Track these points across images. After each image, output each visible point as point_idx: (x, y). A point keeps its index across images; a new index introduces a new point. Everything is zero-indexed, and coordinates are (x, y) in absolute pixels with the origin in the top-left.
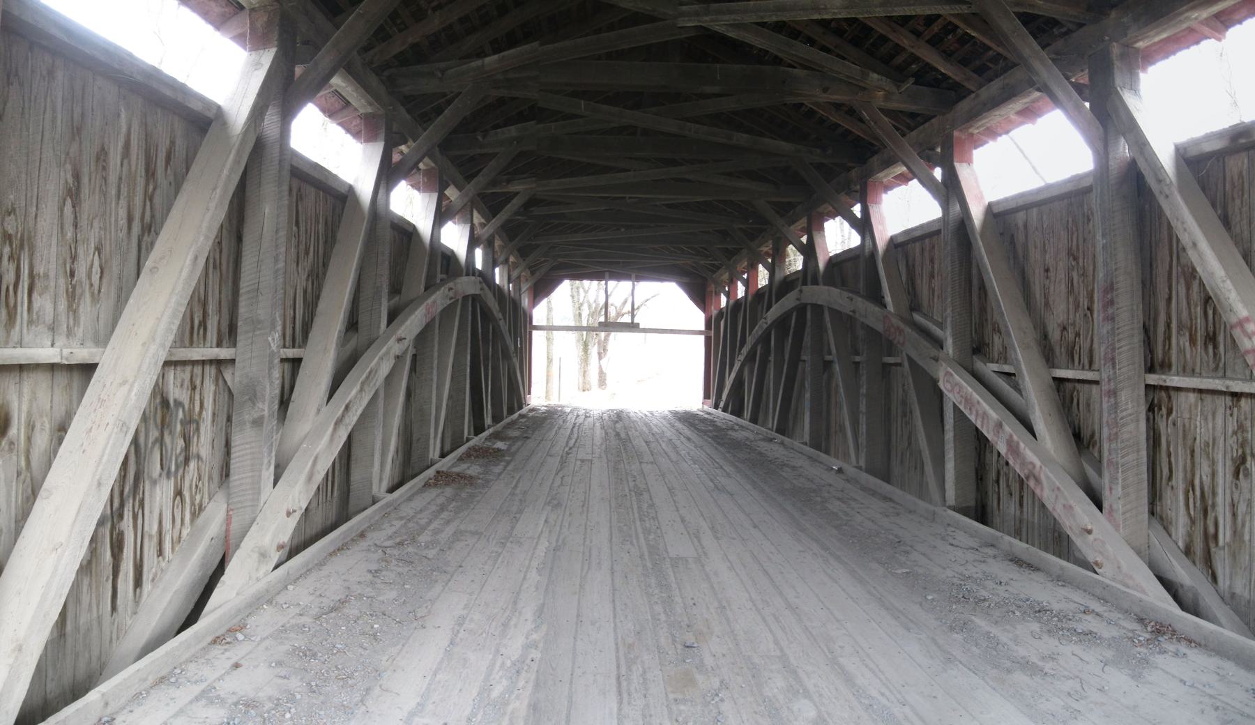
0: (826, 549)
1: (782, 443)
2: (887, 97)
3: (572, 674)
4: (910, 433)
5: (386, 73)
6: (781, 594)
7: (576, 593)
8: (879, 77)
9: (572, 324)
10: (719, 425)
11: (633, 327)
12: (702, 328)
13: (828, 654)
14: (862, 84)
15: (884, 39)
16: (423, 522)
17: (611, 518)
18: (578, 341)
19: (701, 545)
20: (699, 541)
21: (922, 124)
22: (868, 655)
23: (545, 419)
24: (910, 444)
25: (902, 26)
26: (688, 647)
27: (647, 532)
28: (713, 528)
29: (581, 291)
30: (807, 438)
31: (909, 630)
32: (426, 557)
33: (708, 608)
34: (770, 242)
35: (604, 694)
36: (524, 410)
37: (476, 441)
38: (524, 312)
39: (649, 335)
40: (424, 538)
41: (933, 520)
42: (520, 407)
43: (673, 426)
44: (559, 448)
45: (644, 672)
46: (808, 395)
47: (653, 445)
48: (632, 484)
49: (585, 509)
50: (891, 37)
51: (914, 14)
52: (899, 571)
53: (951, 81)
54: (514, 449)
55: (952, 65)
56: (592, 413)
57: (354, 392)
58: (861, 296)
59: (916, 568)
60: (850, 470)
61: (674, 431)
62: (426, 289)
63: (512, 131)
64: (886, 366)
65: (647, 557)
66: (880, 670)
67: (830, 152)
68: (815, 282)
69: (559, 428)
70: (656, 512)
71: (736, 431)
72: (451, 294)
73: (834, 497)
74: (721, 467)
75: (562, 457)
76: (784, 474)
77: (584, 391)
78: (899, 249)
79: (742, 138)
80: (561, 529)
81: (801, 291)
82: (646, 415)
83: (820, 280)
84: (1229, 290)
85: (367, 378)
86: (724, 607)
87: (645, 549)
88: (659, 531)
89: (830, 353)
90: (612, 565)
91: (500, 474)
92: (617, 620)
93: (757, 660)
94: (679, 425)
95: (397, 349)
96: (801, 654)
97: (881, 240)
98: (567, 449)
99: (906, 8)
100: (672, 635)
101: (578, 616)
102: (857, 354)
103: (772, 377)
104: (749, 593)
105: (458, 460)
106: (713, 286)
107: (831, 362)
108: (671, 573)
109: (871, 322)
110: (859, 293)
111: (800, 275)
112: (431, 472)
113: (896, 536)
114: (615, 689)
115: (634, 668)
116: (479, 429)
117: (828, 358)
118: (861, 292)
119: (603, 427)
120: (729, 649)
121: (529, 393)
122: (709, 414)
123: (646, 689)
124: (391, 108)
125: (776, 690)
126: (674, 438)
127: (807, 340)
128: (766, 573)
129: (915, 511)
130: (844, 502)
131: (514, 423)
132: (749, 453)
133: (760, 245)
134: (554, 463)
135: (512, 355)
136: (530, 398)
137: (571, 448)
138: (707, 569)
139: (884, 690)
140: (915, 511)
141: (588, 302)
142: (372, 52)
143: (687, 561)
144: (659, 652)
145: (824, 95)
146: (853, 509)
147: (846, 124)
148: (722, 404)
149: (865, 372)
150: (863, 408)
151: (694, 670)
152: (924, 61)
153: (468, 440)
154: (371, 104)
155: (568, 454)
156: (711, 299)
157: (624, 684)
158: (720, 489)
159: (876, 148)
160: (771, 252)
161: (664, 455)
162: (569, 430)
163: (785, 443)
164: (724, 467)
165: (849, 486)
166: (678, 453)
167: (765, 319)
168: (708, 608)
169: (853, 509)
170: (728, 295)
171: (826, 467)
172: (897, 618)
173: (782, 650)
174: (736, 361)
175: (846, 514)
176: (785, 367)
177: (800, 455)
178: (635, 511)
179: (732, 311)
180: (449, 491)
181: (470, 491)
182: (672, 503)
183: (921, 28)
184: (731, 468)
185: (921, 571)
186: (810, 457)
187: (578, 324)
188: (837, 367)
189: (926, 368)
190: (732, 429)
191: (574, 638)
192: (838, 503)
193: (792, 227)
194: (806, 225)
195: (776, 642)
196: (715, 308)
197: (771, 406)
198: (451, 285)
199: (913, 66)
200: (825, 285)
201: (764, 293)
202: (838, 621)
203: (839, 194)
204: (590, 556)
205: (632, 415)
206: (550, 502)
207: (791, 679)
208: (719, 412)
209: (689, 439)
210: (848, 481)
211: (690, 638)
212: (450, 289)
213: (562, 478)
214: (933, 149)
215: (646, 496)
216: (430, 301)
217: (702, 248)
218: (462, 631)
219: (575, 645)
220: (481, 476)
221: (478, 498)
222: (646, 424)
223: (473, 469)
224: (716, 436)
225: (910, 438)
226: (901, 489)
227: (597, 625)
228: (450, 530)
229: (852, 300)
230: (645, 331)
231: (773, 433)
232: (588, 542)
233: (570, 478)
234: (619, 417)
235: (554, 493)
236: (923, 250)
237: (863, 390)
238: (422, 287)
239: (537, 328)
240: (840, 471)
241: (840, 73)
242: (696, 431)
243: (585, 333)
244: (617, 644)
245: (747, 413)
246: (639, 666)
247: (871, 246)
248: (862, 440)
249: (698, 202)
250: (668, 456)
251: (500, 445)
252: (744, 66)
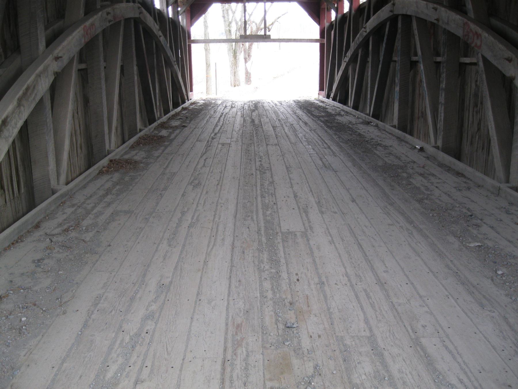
0: (411, 222)
1: (377, 126)
3: (183, 359)
4: (480, 120)
6: (372, 268)
7: (199, 270)
9: (225, 38)
10: (330, 111)
11: (266, 38)
12: (318, 37)
13: (411, 334)
16: (89, 207)
17: (238, 196)
18: (229, 50)
19: (308, 219)
20: (307, 216)
22: (447, 336)
23: (201, 110)
24: (479, 129)
26: (288, 327)
27: (265, 207)
28: (319, 203)
29: (230, 12)
30: (396, 122)
31: (482, 306)
32: (83, 240)
33: (309, 285)
35: (209, 381)
36: (187, 104)
37: (146, 131)
38: (183, 28)
39: (283, 44)
40: (85, 223)
41: (498, 195)
42: (184, 102)
43: (295, 113)
44: (206, 136)
45: (247, 356)
46: (397, 89)
47: (278, 130)
48: (258, 164)
49: (219, 187)
52: (472, 245)
54: (173, 136)
56: (236, 104)
57: (10, 108)
59: (486, 241)
60: (430, 149)
61: (295, 117)
62: (86, 14)
64: (463, 66)
65: (262, 232)
66: (458, 353)
69: (210, 117)
70: (275, 189)
71: (342, 116)
72: (110, 17)
73: (417, 173)
74: (329, 148)
75: (208, 142)
76: (377, 152)
77: (235, 86)
80: (197, 206)
82: (276, 105)
84: (160, 36)
85: (25, 94)
86: (323, 283)
87: (262, 224)
88: (275, 207)
89: (416, 55)
90: (234, 241)
91: (158, 157)
92: (231, 298)
93: (348, 342)
94: (300, 112)
95: (55, 67)
96: (388, 334)
98: (213, 135)
100: (276, 314)
101: (198, 294)
102: (438, 55)
103: (369, 74)
104: (345, 268)
105: (130, 148)
106: (325, 4)
107: (416, 62)
108: (281, 247)
109: (453, 28)
112: (105, 162)
113: (469, 210)
114: (219, 376)
115: (239, 351)
116: (152, 120)
117: (414, 59)
118: (445, 3)
119: (242, 116)
120: (325, 329)
121: (191, 90)
122: (323, 102)
123: (247, 376)
125: (364, 377)
126: (295, 123)
127: (398, 44)
128: (360, 246)
129: (483, 186)
130: (425, 178)
131: (177, 114)
132: (351, 135)
134: (200, 147)
135: (173, 63)
136: (192, 95)
137: (216, 134)
138: (312, 243)
139: (462, 376)
140: (483, 186)
141: (236, 20)
143: (295, 235)
144: (263, 333)
146: (432, 184)
148: (332, 95)
149: (445, 70)
150: (442, 99)
151: (292, 353)
153: (141, 130)
155: (213, 139)
156: (325, 15)
157: (228, 369)
158: (327, 167)
161: (286, 137)
162: (218, 119)
163: (379, 126)
164: (331, 147)
165: (429, 162)
166: (296, 135)
167: (365, 28)
168: (309, 285)
169: (432, 184)
170: (337, 11)
171: (410, 147)
172: (471, 293)
173: (371, 330)
174: (343, 62)
175: (427, 189)
176: (380, 66)
177: (390, 136)
178: (258, 188)
180: (116, 176)
181: (132, 174)
182: (288, 180)
184: (336, 148)
185: (490, 244)
186: (398, 138)
187: (229, 38)
188: (421, 67)
189: (500, 68)
190: (339, 114)
191: (192, 318)
192: (420, 178)
195: (366, 321)
196: (327, 22)
197: (369, 97)
198: (109, 10)
201: (364, 8)
202: (421, 297)
204: (217, 231)
205: (266, 105)
206: (192, 182)
207: (378, 364)
208: (330, 101)
209: (306, 124)
210: (428, 158)
211: (291, 316)
212: (108, 14)
213: (205, 160)
215: (268, 174)
216: (88, 23)
218: (96, 312)
219: (190, 326)
220: (144, 161)
221: (137, 180)
222: (275, 112)
223: (139, 155)
224: (327, 120)
225: (479, 124)
226: (470, 166)
227: (213, 303)
228: (109, 211)
230: (275, 40)
231: (370, 118)
232: (216, 219)
233: (212, 159)
234: (256, 106)
235: (197, 173)
237: (443, 85)
238: (82, 12)
239: (194, 42)
240: (422, 149)
242: (311, 117)
243: (234, 44)
244: (227, 324)
245: (351, 101)
246: (244, 349)
248: (441, 125)
250: (289, 139)
251: (164, 133)
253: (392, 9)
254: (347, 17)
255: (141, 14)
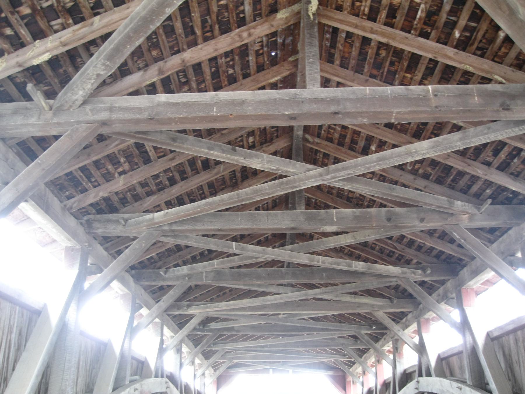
2: (472, 217)
5: (85, 218)
8: (463, 203)
14: (450, 211)
15: (461, 174)
21: (500, 237)
25: (475, 160)
34: (391, 343)
50: (468, 171)
51: (488, 141)
53: (520, 197)
55: (520, 183)
58: (469, 386)
63: (185, 270)
67: (429, 272)
68: (429, 374)
78: (496, 342)
79: (359, 266)
81: (418, 382)
83: (433, 372)
99: (481, 138)
110: (466, 382)
118: (468, 382)
124: (87, 244)
133: (383, 346)
142: (72, 200)
145: (422, 224)
147: (440, 246)
152: (496, 184)
154: (69, 240)
156: (351, 388)
159: (464, 262)
160: (392, 350)
183: (490, 159)
193: (406, 331)
194: (416, 329)
198: (137, 386)
199: (488, 191)
200: (437, 376)
201: (389, 383)
203: (439, 303)
214: (513, 255)
229: (461, 389)
236: (516, 341)
241: (432, 205)
247: (471, 342)
249: (333, 315)
252: (354, 210)
253: (417, 386)
254: (373, 391)
255: (168, 389)
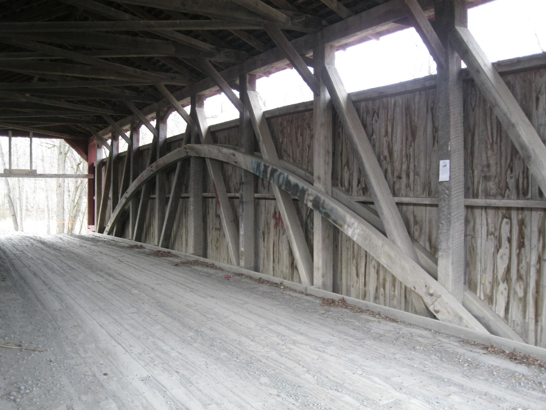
83: (202, 140)
97: (258, 113)
111: (126, 154)
133: (104, 135)
148: (107, 229)
179: (115, 163)
217: (188, 33)
